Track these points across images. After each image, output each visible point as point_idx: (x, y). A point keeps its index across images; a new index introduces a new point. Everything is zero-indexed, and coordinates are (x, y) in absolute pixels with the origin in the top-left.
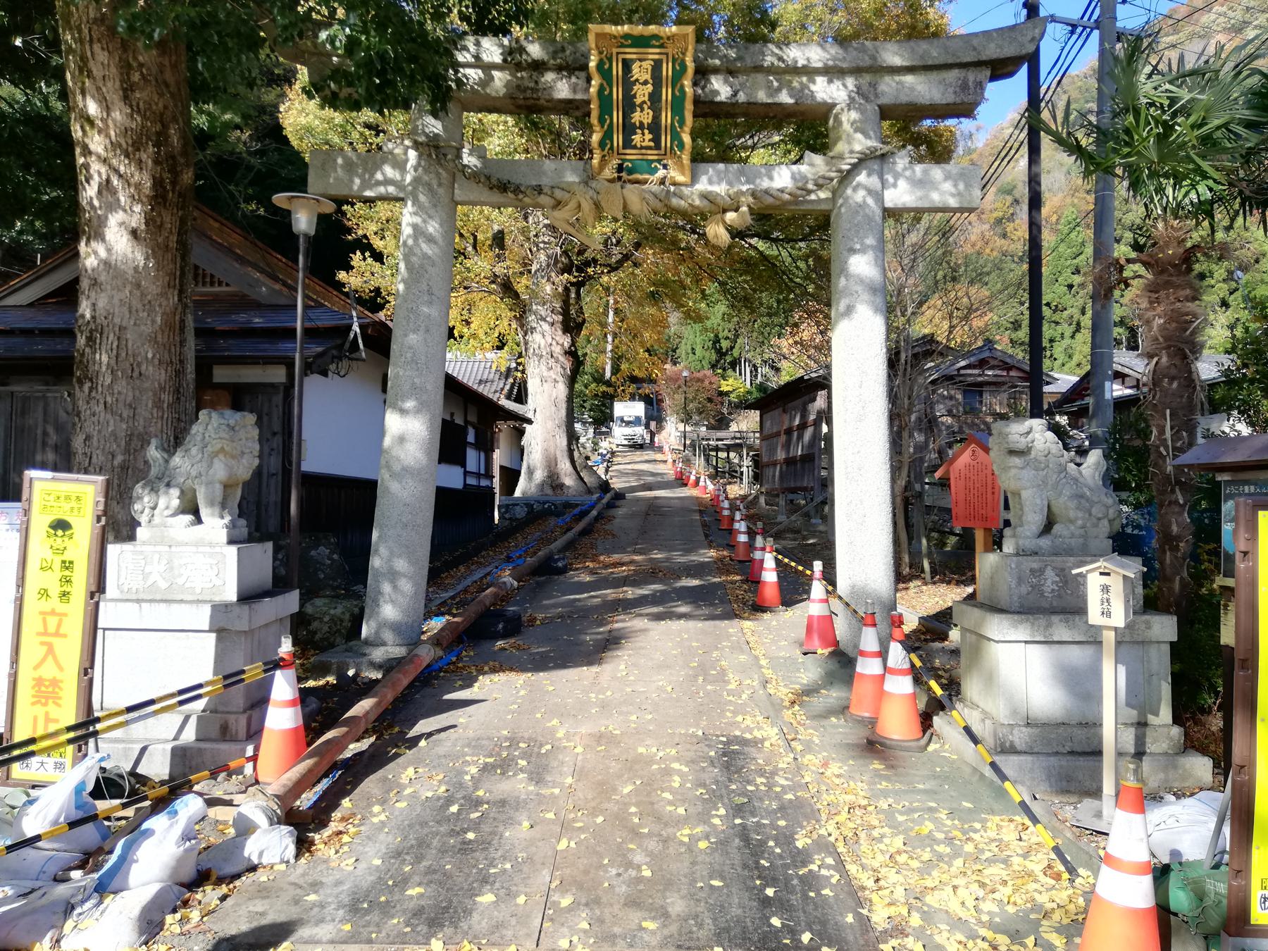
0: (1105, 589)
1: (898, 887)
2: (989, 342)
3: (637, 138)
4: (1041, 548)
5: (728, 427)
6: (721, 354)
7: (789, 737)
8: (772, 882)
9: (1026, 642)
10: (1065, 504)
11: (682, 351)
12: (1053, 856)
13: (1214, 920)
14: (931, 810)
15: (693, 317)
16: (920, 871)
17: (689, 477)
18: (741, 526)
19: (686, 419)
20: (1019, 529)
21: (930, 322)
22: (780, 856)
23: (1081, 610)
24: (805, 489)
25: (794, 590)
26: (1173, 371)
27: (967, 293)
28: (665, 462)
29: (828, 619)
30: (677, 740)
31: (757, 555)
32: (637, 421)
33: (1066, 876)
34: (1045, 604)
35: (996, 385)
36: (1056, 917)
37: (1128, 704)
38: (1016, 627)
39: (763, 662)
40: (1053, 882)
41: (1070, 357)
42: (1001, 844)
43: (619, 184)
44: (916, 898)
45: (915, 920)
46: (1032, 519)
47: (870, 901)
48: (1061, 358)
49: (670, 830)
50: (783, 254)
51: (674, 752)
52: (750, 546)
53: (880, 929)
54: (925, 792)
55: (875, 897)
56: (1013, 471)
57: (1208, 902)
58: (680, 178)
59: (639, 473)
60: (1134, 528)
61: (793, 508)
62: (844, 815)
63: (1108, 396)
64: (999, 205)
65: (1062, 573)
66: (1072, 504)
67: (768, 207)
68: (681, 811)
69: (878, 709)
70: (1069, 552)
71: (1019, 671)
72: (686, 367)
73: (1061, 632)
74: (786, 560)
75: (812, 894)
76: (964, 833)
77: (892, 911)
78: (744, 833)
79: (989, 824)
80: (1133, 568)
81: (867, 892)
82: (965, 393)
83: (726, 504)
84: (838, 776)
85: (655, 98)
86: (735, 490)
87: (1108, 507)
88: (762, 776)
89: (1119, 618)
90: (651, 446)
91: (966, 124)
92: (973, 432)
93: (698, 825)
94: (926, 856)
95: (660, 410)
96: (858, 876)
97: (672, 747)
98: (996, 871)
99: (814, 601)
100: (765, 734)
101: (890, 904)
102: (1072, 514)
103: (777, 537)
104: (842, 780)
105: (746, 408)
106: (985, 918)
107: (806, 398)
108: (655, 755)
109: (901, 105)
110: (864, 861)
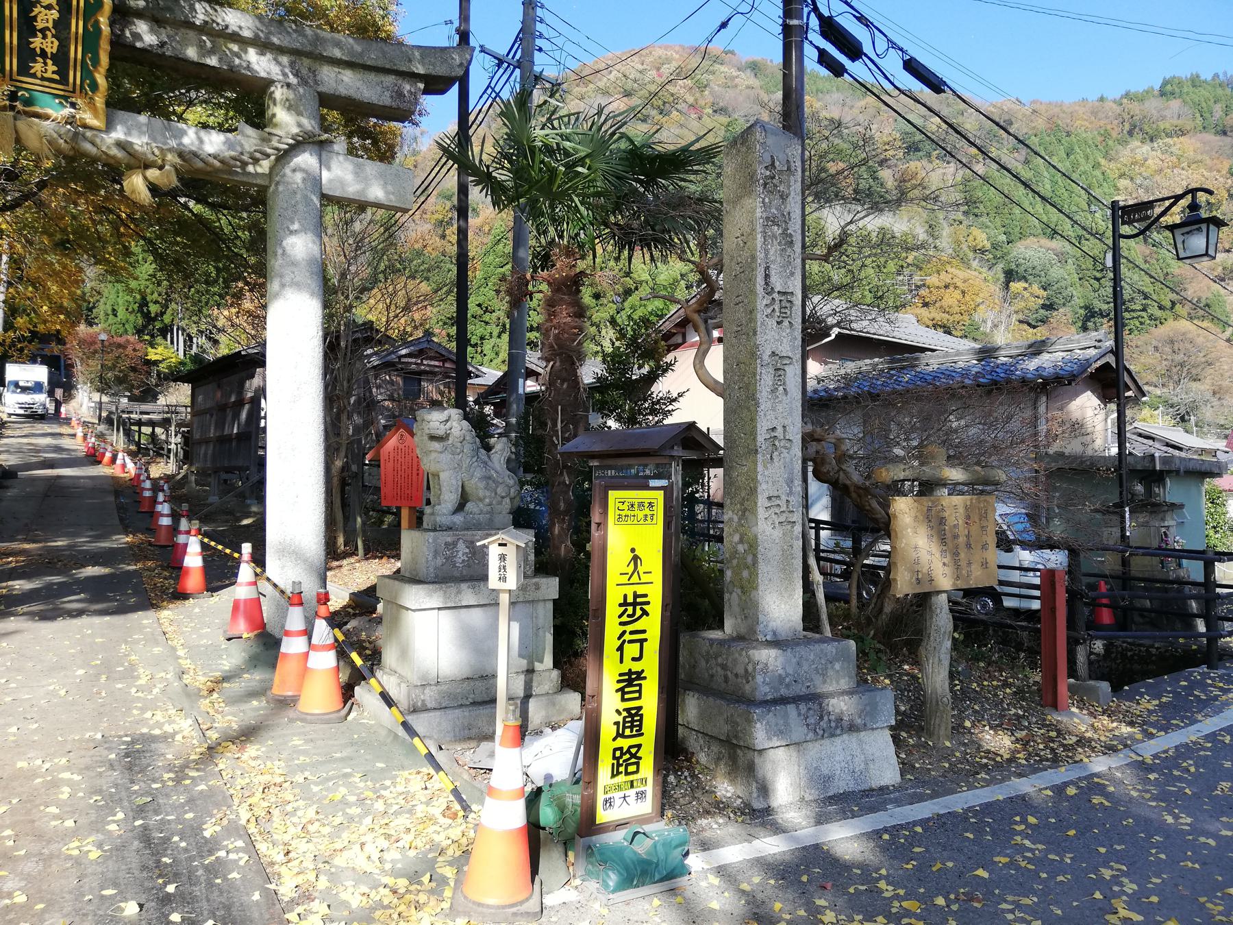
0: (503, 557)
1: (308, 855)
2: (428, 334)
3: (37, 67)
4: (455, 524)
5: (155, 399)
6: (149, 318)
7: (205, 727)
8: (176, 877)
9: (439, 609)
10: (476, 485)
11: (100, 310)
12: (452, 798)
13: (571, 827)
14: (346, 776)
15: (113, 272)
16: (330, 835)
17: (103, 455)
18: (164, 508)
19: (103, 386)
20: (437, 507)
21: (370, 311)
22: (186, 850)
23: (485, 578)
24: (240, 469)
25: (219, 574)
26: (564, 374)
27: (405, 287)
28: (74, 435)
29: (256, 603)
30: (69, 747)
31: (181, 539)
32: (37, 388)
33: (461, 813)
34: (456, 574)
35: (431, 374)
36: (450, 852)
37: (520, 656)
38: (431, 596)
39: (181, 653)
40: (450, 821)
41: (497, 354)
42: (407, 796)
43: (11, 113)
44: (324, 862)
45: (323, 883)
46: (449, 498)
47: (279, 875)
48: (490, 355)
49: (54, 847)
50: (224, 221)
51: (64, 760)
52: (174, 530)
53: (286, 899)
54: (342, 759)
55: (283, 870)
56: (434, 455)
57: (568, 812)
58: (94, 122)
59: (37, 450)
60: (537, 504)
61: (227, 487)
62: (259, 795)
63: (521, 391)
64: (439, 208)
65: (471, 544)
66: (482, 485)
67: (198, 171)
68: (69, 823)
69: (300, 686)
70: (478, 527)
71: (430, 636)
72: (104, 330)
73: (468, 597)
74: (213, 544)
75: (218, 881)
76: (375, 792)
77: (299, 880)
78: (145, 836)
79: (398, 780)
80: (526, 538)
81: (276, 867)
82: (405, 379)
83: (148, 484)
84: (255, 759)
85: (62, 25)
86: (157, 471)
87: (510, 488)
88: (170, 771)
89: (512, 583)
90: (56, 417)
91: (406, 129)
92: (404, 420)
93: (90, 835)
94: (338, 820)
95: (70, 376)
96: (268, 853)
97: (62, 756)
98: (403, 821)
99: (241, 585)
100: (176, 727)
101: (298, 873)
102: (481, 494)
103: (204, 520)
104: (259, 762)
105: (175, 381)
106: (388, 866)
107: (244, 374)
108: (40, 767)
109: (339, 97)
110: (275, 837)
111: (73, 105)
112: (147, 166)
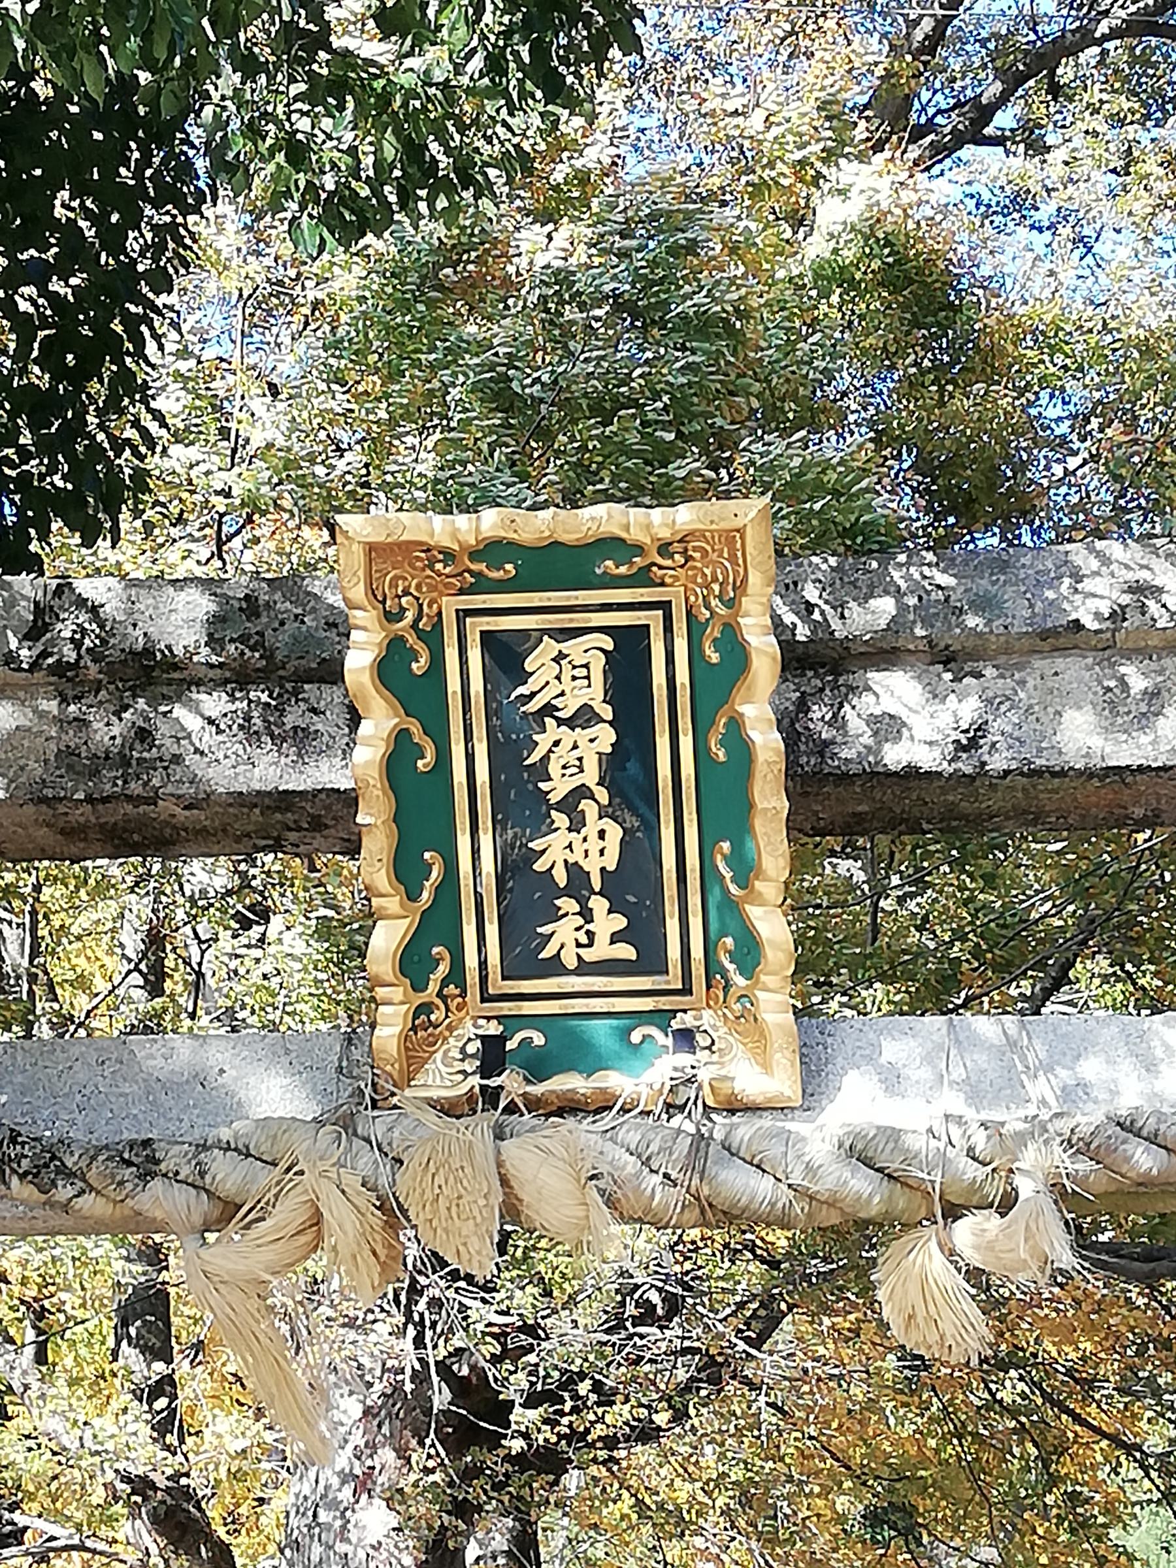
3: (563, 935)
58: (750, 1081)
111: (686, 1038)
112: (953, 1212)
